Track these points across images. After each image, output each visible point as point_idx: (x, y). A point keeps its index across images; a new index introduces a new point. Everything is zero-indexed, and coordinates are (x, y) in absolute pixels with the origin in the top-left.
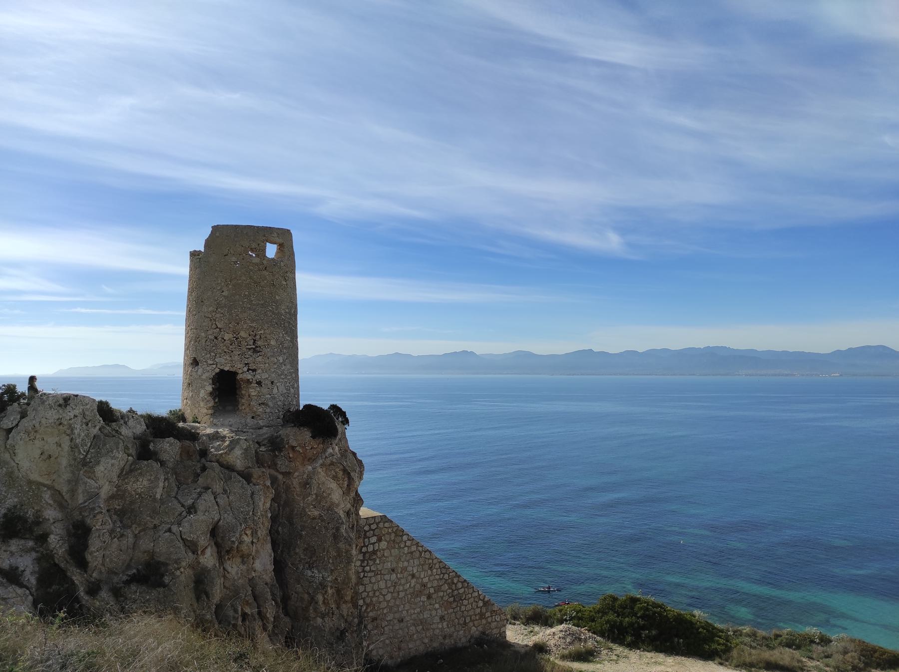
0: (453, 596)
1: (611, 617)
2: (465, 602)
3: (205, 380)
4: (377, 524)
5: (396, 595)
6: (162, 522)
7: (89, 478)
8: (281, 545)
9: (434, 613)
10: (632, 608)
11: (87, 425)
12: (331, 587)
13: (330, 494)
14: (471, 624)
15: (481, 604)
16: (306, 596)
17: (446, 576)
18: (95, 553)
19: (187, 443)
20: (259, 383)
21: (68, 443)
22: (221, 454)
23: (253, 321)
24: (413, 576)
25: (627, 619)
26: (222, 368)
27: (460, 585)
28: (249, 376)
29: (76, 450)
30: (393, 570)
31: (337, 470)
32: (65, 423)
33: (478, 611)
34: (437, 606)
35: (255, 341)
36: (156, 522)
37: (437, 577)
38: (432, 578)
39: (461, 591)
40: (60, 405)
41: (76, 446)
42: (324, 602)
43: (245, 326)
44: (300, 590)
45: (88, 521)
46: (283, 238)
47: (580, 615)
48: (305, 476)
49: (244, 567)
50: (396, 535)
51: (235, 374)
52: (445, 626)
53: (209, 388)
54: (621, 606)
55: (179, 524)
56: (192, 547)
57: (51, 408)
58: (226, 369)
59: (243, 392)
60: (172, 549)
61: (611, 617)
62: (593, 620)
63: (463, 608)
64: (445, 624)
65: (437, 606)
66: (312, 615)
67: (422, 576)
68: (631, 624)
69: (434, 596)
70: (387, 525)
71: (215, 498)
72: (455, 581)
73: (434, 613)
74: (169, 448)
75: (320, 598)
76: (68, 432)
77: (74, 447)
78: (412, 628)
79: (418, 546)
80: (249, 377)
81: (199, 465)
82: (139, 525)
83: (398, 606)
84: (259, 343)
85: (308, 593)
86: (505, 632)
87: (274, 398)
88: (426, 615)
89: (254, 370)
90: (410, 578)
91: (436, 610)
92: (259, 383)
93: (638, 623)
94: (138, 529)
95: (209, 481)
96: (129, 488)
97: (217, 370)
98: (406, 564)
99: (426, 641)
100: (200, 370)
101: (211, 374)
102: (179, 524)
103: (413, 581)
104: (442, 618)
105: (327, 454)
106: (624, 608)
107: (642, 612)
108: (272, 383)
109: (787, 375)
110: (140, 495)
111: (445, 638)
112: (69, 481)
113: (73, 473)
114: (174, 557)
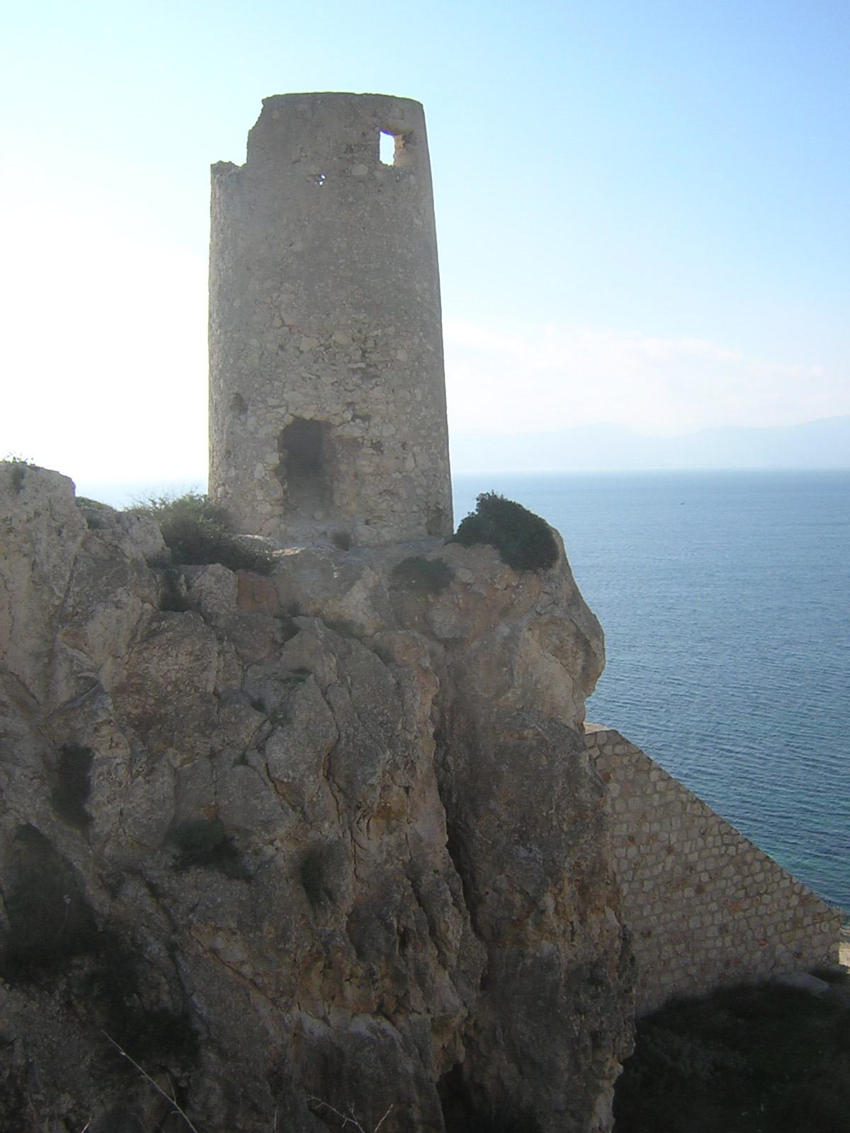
0: (744, 888)
2: (766, 899)
4: (601, 747)
5: (636, 885)
7: (75, 647)
9: (708, 920)
11: (60, 533)
12: (570, 880)
13: (548, 688)
14: (776, 938)
15: (795, 901)
17: (732, 850)
18: (104, 806)
20: (377, 446)
24: (670, 850)
26: (298, 413)
27: (757, 866)
28: (355, 430)
30: (632, 839)
31: (564, 635)
32: (20, 528)
33: (790, 913)
34: (713, 906)
35: (364, 352)
37: (715, 851)
38: (705, 853)
39: (760, 877)
42: (556, 911)
44: (505, 885)
46: (405, 118)
49: (391, 840)
50: (638, 771)
51: (328, 426)
52: (728, 943)
53: (274, 459)
56: (293, 795)
58: (308, 415)
59: (343, 468)
63: (762, 910)
64: (728, 939)
65: (713, 906)
67: (687, 851)
69: (709, 888)
70: (618, 749)
71: (324, 693)
72: (749, 858)
73: (708, 920)
74: (212, 581)
75: (549, 901)
77: (40, 582)
78: (668, 948)
79: (679, 791)
80: (357, 433)
83: (641, 907)
84: (374, 357)
86: (837, 953)
88: (693, 923)
89: (366, 418)
90: (663, 853)
91: (713, 913)
92: (377, 446)
96: (153, 671)
97: (289, 420)
98: (656, 827)
99: (693, 970)
100: (252, 421)
101: (276, 429)
103: (670, 859)
104: (723, 929)
108: (404, 445)
110: (175, 684)
111: (727, 964)
112: (37, 656)
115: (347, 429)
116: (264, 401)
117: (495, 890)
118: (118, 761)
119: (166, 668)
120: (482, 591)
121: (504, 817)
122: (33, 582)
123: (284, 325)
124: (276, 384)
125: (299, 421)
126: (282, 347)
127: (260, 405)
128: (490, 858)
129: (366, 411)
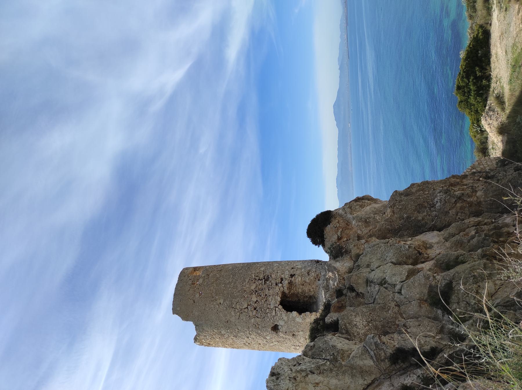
1: (472, 100)
3: (288, 318)
6: (393, 300)
8: (419, 229)
10: (464, 87)
16: (458, 205)
19: (332, 309)
21: (315, 376)
22: (339, 275)
23: (245, 281)
25: (471, 87)
26: (278, 303)
28: (286, 282)
29: (322, 368)
32: (294, 375)
36: (393, 304)
40: (277, 379)
41: (318, 367)
43: (248, 286)
45: (390, 351)
47: (475, 122)
48: (360, 224)
54: (464, 95)
55: (395, 285)
57: (278, 385)
59: (300, 291)
60: (416, 284)
61: (472, 100)
62: (477, 111)
66: (475, 199)
68: (474, 84)
76: (304, 374)
80: (287, 282)
81: (349, 294)
82: (396, 318)
85: (456, 203)
87: (305, 267)
92: (292, 276)
93: (473, 80)
94: (400, 319)
95: (360, 281)
96: (363, 331)
97: (280, 307)
101: (284, 312)
102: (395, 285)
105: (343, 213)
106: (465, 92)
107: (465, 79)
109: (351, 148)
112: (353, 376)
113: (344, 373)
114: (423, 281)
115: (284, 285)
116: (274, 317)
117: (457, 215)
118: (400, 338)
119: (361, 326)
120: (340, 231)
121: (425, 214)
122: (319, 374)
123: (247, 308)
124: (267, 311)
125: (281, 303)
126: (255, 309)
127: (275, 318)
128: (443, 217)
129: (279, 279)
